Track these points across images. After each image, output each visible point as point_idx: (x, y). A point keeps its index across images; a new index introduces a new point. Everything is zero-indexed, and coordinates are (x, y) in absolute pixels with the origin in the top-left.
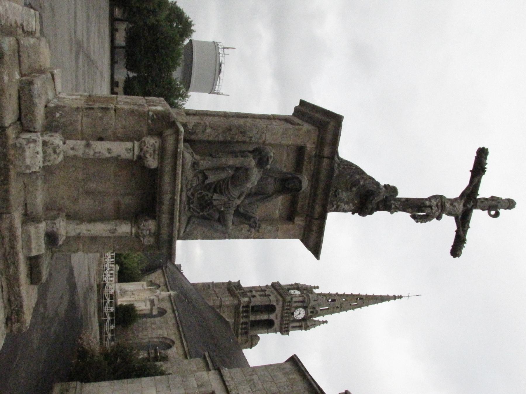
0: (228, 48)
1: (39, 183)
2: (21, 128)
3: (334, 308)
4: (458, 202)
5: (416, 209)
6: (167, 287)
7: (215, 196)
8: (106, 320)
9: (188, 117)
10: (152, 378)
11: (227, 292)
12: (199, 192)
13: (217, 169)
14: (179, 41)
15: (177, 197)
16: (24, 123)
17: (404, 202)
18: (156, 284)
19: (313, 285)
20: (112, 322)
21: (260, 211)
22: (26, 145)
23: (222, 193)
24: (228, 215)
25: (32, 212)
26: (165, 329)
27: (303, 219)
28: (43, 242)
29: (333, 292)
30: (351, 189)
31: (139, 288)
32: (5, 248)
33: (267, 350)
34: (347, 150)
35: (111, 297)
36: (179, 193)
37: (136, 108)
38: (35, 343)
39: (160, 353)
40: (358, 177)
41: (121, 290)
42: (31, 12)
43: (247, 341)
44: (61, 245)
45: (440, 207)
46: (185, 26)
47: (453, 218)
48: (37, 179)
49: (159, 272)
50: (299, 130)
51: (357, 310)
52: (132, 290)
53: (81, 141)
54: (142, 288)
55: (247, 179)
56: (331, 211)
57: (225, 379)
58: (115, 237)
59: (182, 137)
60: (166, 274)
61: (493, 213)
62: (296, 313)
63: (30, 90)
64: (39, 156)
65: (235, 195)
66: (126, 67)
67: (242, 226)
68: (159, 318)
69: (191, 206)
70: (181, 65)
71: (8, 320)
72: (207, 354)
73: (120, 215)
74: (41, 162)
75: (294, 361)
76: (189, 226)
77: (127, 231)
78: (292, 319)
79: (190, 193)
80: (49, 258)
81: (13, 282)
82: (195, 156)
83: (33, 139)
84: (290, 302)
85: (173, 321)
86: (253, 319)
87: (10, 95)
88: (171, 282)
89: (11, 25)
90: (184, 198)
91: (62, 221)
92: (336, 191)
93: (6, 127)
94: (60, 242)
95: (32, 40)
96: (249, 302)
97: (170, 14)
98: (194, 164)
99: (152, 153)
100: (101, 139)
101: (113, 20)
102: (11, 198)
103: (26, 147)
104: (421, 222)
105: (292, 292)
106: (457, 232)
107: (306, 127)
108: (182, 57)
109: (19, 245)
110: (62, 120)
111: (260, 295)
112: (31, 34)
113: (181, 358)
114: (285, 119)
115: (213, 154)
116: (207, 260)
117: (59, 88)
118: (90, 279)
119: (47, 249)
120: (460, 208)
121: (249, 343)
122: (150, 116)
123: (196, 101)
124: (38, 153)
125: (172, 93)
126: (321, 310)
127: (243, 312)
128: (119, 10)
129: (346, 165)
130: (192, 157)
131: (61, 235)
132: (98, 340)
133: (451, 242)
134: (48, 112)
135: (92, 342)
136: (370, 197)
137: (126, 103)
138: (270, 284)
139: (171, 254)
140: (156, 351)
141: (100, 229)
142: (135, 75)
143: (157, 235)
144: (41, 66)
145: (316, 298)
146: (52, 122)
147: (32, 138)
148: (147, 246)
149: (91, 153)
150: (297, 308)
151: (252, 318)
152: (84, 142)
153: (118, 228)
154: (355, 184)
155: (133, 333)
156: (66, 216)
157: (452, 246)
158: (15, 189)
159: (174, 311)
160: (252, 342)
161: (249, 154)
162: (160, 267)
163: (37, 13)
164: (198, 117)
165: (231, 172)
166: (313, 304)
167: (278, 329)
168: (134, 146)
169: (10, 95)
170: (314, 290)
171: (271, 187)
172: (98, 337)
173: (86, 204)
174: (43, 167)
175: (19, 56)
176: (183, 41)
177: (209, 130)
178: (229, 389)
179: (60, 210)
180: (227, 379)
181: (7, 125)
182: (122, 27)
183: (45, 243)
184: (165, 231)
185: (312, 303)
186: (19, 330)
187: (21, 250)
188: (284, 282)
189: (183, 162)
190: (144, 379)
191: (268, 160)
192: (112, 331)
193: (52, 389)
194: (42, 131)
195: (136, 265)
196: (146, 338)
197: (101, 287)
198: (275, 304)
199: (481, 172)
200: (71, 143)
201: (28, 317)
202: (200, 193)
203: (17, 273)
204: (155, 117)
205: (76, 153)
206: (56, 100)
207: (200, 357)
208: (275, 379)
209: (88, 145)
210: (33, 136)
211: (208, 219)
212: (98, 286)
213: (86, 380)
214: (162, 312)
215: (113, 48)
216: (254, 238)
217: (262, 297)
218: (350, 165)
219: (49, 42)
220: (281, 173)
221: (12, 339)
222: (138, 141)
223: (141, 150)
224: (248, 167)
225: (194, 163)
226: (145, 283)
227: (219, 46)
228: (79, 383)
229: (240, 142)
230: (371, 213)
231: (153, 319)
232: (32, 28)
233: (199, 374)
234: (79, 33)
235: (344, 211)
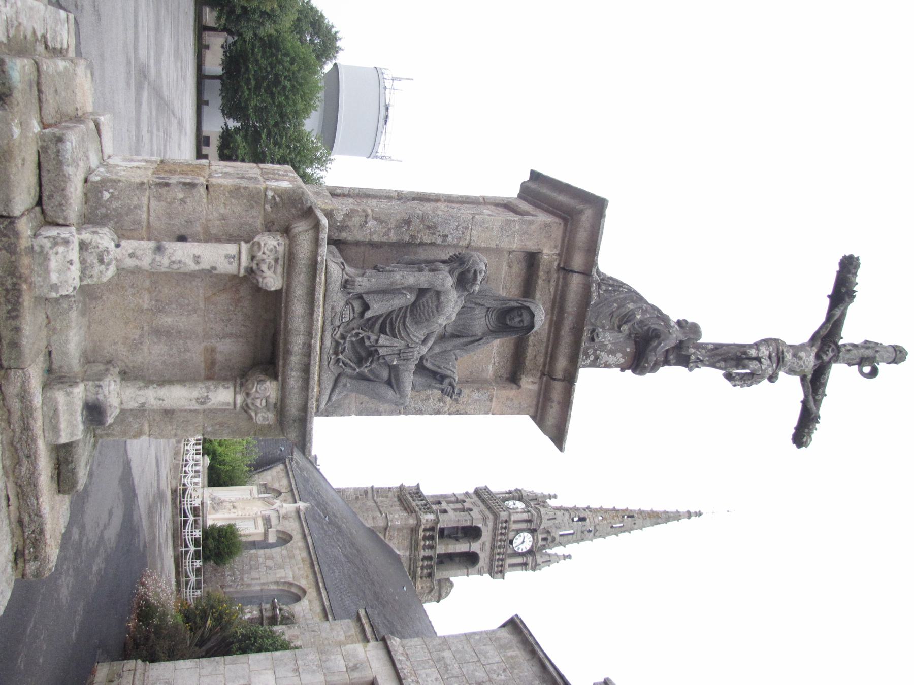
0: (400, 79)
1: (74, 314)
2: (42, 218)
3: (583, 532)
4: (806, 351)
5: (734, 363)
6: (293, 496)
7: (383, 340)
8: (187, 552)
9: (335, 200)
10: (268, 653)
11: (397, 503)
12: (354, 332)
14: (315, 65)
16: (46, 209)
17: (713, 350)
18: (274, 490)
19: (546, 493)
20: (197, 555)
21: (460, 365)
22: (51, 248)
23: (394, 336)
24: (406, 374)
25: (61, 367)
26: (289, 568)
27: (536, 380)
28: (80, 418)
29: (582, 505)
30: (619, 327)
31: (245, 497)
32: (14, 431)
33: (468, 606)
34: (611, 261)
35: (196, 511)
37: (244, 183)
38: (64, 593)
39: (281, 610)
40: (631, 306)
41: (213, 499)
42: (59, 14)
43: (431, 590)
44: (111, 425)
45: (775, 359)
46: (327, 43)
47: (797, 379)
48: (70, 308)
49: (280, 467)
50: (531, 223)
51: (624, 536)
52: (233, 499)
53: (148, 242)
54: (249, 497)
55: (439, 308)
56: (584, 366)
57: (394, 657)
58: (204, 411)
59: (324, 236)
60: (290, 473)
61: (867, 369)
62: (517, 542)
63: (58, 151)
64: (73, 268)
65: (417, 337)
66: (223, 111)
67: (429, 392)
68: (278, 549)
69: (341, 356)
70: (318, 109)
71: (18, 555)
72: (362, 613)
73: (213, 373)
74: (77, 279)
75: (515, 625)
76: (337, 391)
77: (227, 401)
78: (509, 551)
79: (338, 335)
80: (89, 447)
81: (25, 490)
82: (347, 268)
83: (63, 239)
84: (506, 522)
85: (305, 554)
86: (443, 551)
87: (24, 160)
88: (301, 486)
89: (25, 37)
90: (328, 343)
91: (113, 383)
92: (593, 331)
93: (15, 217)
94: (110, 420)
95: (62, 64)
96: (437, 521)
97: (299, 20)
98: (346, 284)
99: (273, 263)
100: (182, 239)
101: (201, 29)
102: (24, 341)
103: (51, 252)
104: (742, 386)
105: (510, 504)
106: (805, 403)
107: (543, 218)
108: (321, 95)
109: (38, 424)
110: (115, 205)
111: (455, 510)
112: (59, 53)
113: (317, 619)
114: (507, 206)
115: (379, 265)
116: (364, 450)
117: (108, 149)
118: (159, 481)
119: (86, 431)
120: (809, 361)
121: (435, 593)
122: (270, 197)
123: (342, 171)
124: (71, 262)
125: (300, 156)
126: (561, 535)
127: (425, 538)
128: (211, 12)
129: (610, 285)
130: (343, 270)
131: (110, 406)
132: (174, 587)
133: (794, 422)
134: (89, 191)
135: (163, 590)
136: (652, 343)
137: (226, 175)
138: (471, 491)
139: (303, 442)
140: (274, 608)
141: (179, 396)
142: (239, 125)
143: (280, 409)
144: (77, 109)
145: (551, 515)
146: (97, 208)
147: (63, 236)
148: (263, 426)
149: (166, 262)
150: (518, 531)
151: (441, 549)
152: (152, 244)
153: (211, 395)
154: (626, 318)
155: (234, 574)
156: (119, 373)
157: (796, 428)
158: (31, 328)
159: (304, 537)
160: (440, 591)
161: (442, 266)
162: (281, 460)
163: (71, 16)
164: (351, 200)
165: (410, 298)
166: (546, 526)
167: (486, 569)
168: (240, 252)
169: (24, 160)
170: (548, 501)
171: (480, 322)
172: (173, 582)
173: (154, 353)
174: (81, 286)
175: (40, 91)
176: (322, 68)
177: (371, 223)
178: (401, 675)
179: (109, 362)
180: (398, 657)
181: (17, 213)
182: (217, 43)
183: (84, 422)
184: (294, 401)
185: (545, 524)
186: (38, 574)
187: (40, 432)
188: (498, 487)
189: (326, 280)
190: (253, 657)
192: (198, 571)
193: (92, 672)
194: (78, 224)
195: (239, 455)
196: (258, 584)
197: (179, 494)
198: (480, 525)
199: (847, 299)
200: (129, 245)
201: (52, 551)
202: (357, 334)
203: (33, 473)
204: (278, 199)
205: (138, 263)
206: (102, 170)
207: (349, 617)
208: (482, 659)
209: (159, 249)
210: (64, 233)
211: (368, 380)
212: (174, 492)
213: (153, 658)
214: (285, 539)
215: (201, 77)
216: (450, 414)
217: (458, 513)
218: (617, 285)
219: (90, 67)
220: (497, 299)
221: (25, 592)
222: (247, 242)
223: (253, 258)
225: (346, 281)
226: (255, 488)
227: (385, 76)
228: (139, 661)
229: (426, 244)
230: (654, 369)
231: (268, 551)
232: (62, 44)
233: (350, 647)
234: (142, 53)
235: (607, 366)
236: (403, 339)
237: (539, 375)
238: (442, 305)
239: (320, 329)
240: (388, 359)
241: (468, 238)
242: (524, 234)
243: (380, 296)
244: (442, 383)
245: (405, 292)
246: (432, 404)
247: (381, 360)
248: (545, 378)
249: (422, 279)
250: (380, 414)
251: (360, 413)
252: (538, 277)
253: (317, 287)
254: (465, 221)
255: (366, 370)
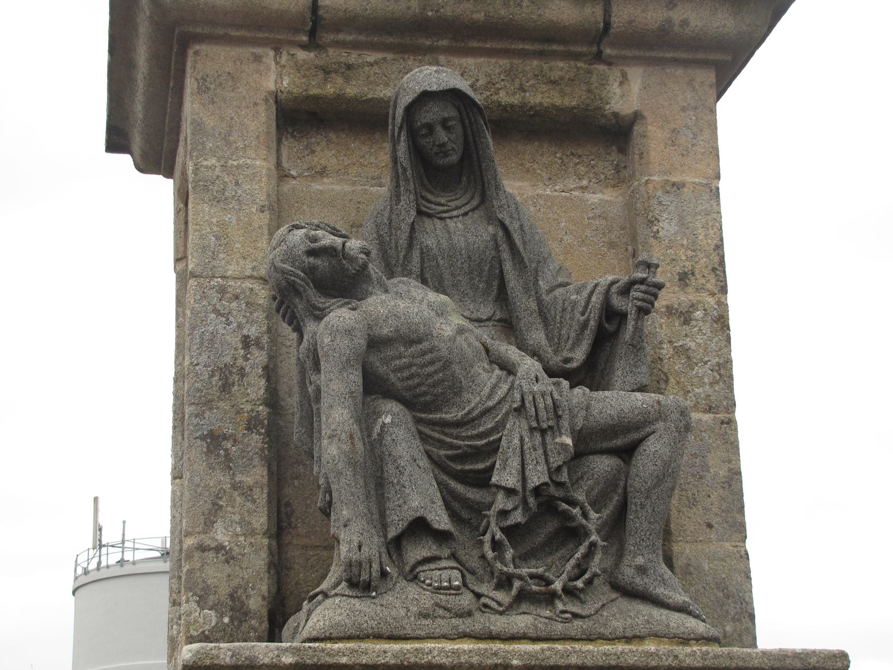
0: (98, 529)
12: (490, 554)
13: (377, 478)
15: (514, 653)
23: (493, 448)
27: (614, 75)
36: (497, 646)
55: (410, 338)
69: (558, 585)
76: (660, 591)
79: (500, 596)
90: (521, 621)
98: (361, 585)
114: (182, 197)
130: (326, 596)
165: (390, 414)
171: (460, 231)
177: (221, 535)
189: (350, 638)
191: (329, 252)
202: (496, 545)
211: (623, 509)
216: (724, 290)
224: (361, 342)
225: (353, 584)
227: (93, 566)
236: (500, 426)
237: (602, 67)
238: (404, 330)
239: (482, 645)
240: (556, 460)
241: (248, 284)
242: (229, 144)
243: (390, 493)
244: (623, 316)
245: (377, 429)
246: (697, 338)
247: (564, 477)
248: (608, 51)
249: (338, 387)
250: (736, 474)
251: (740, 529)
252: (339, 98)
253: (364, 660)
254: (204, 296)
255: (593, 515)
